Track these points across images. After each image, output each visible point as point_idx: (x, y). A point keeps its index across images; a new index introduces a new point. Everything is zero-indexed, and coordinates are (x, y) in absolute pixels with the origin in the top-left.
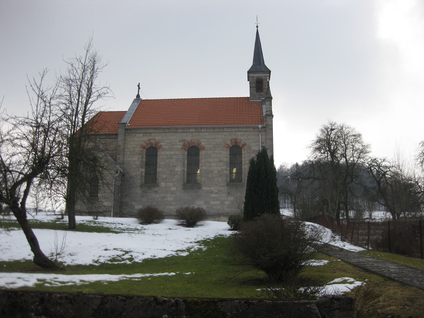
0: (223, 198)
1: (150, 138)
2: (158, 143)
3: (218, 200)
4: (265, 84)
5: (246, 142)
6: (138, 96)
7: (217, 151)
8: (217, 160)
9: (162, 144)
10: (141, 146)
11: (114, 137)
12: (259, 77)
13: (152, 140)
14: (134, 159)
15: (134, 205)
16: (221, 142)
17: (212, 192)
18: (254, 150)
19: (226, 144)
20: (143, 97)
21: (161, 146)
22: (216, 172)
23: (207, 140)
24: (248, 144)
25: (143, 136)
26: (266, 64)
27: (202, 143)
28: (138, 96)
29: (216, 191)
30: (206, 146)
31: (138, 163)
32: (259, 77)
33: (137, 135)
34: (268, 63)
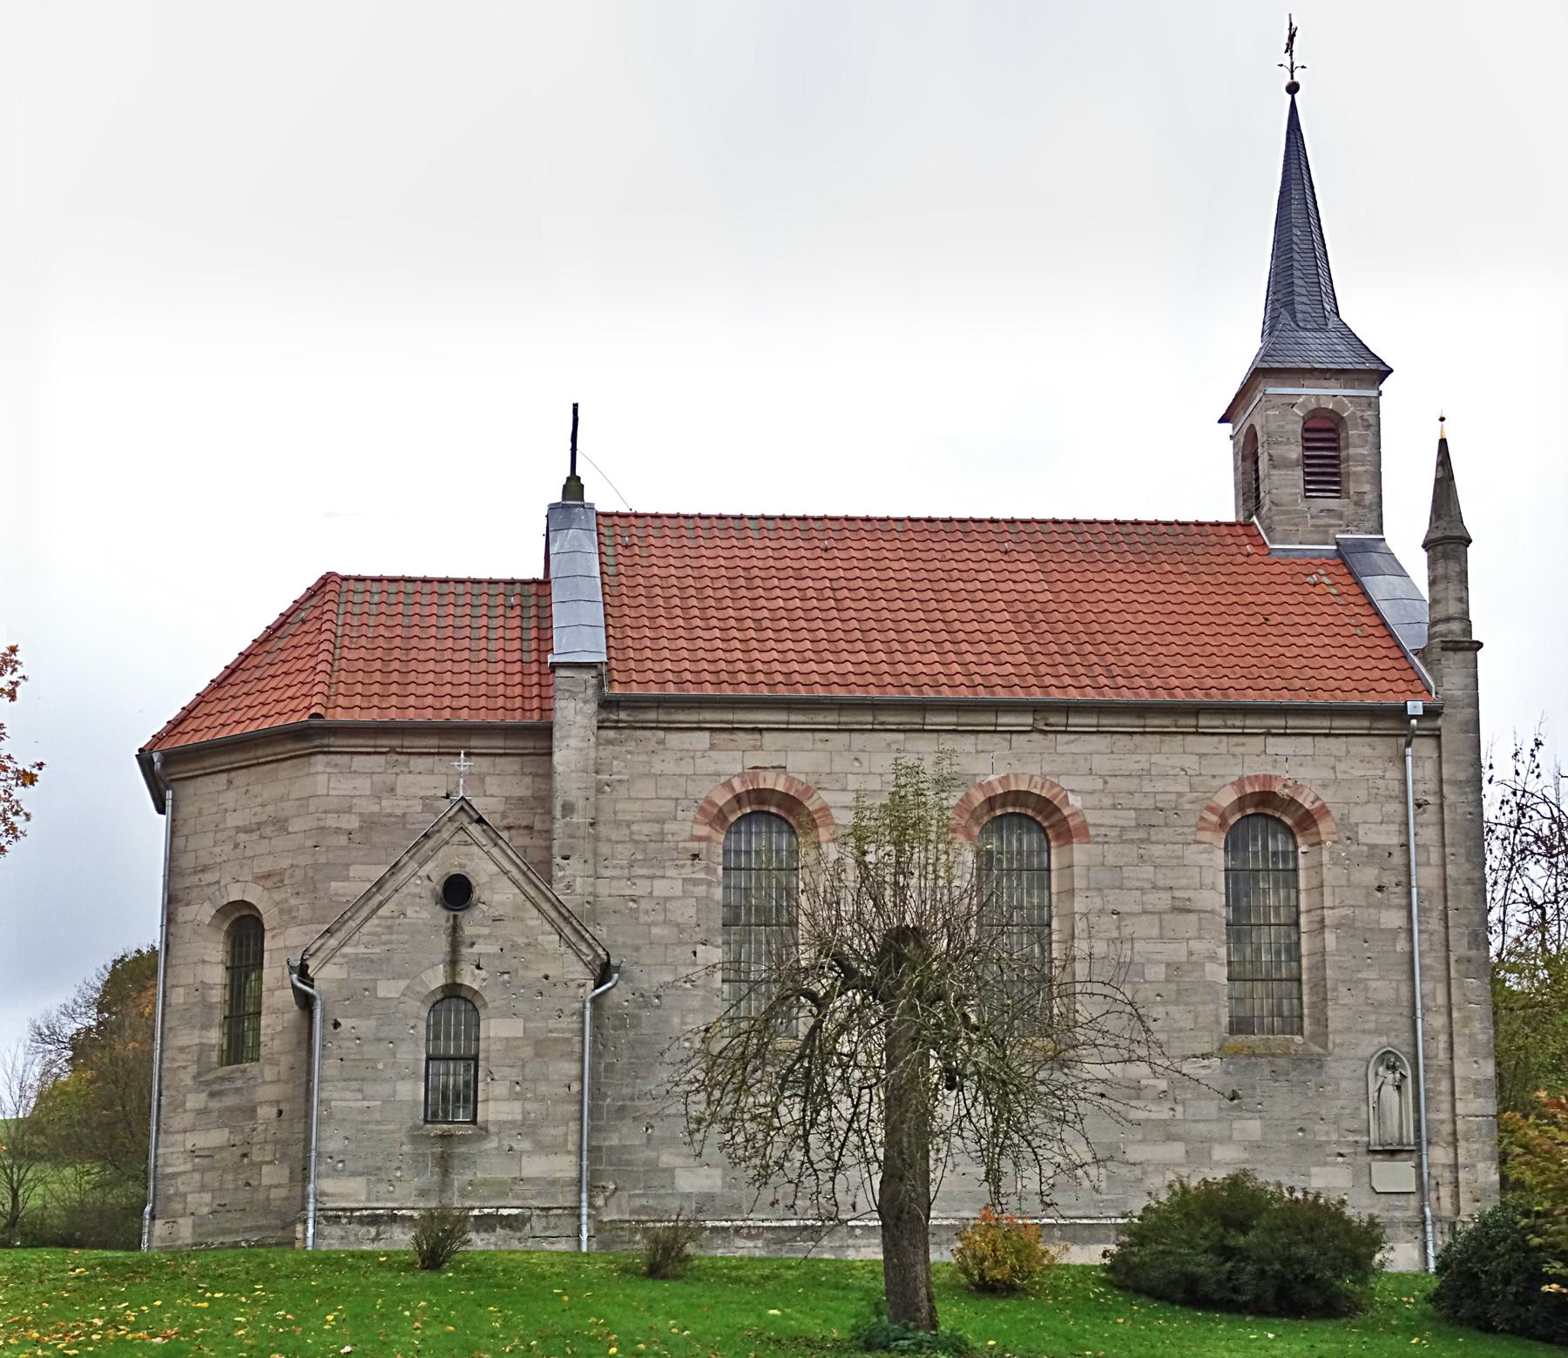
0: (1202, 1128)
1: (754, 759)
2: (808, 791)
3: (1170, 1138)
4: (1356, 449)
5: (1326, 797)
6: (573, 487)
7: (1157, 850)
8: (1162, 900)
9: (827, 797)
10: (702, 810)
11: (529, 744)
12: (1311, 399)
13: (771, 775)
14: (660, 888)
15: (671, 1171)
16: (1180, 795)
17: (1137, 1090)
18: (1372, 847)
19: (1211, 809)
20: (600, 497)
21: (825, 809)
22: (1157, 972)
23: (1099, 784)
24: (1335, 813)
25: (713, 747)
26: (1350, 313)
27: (1071, 798)
28: (573, 487)
29: (1163, 1084)
30: (1091, 817)
31: (686, 912)
32: (1311, 399)
33: (674, 739)
34: (1366, 305)
